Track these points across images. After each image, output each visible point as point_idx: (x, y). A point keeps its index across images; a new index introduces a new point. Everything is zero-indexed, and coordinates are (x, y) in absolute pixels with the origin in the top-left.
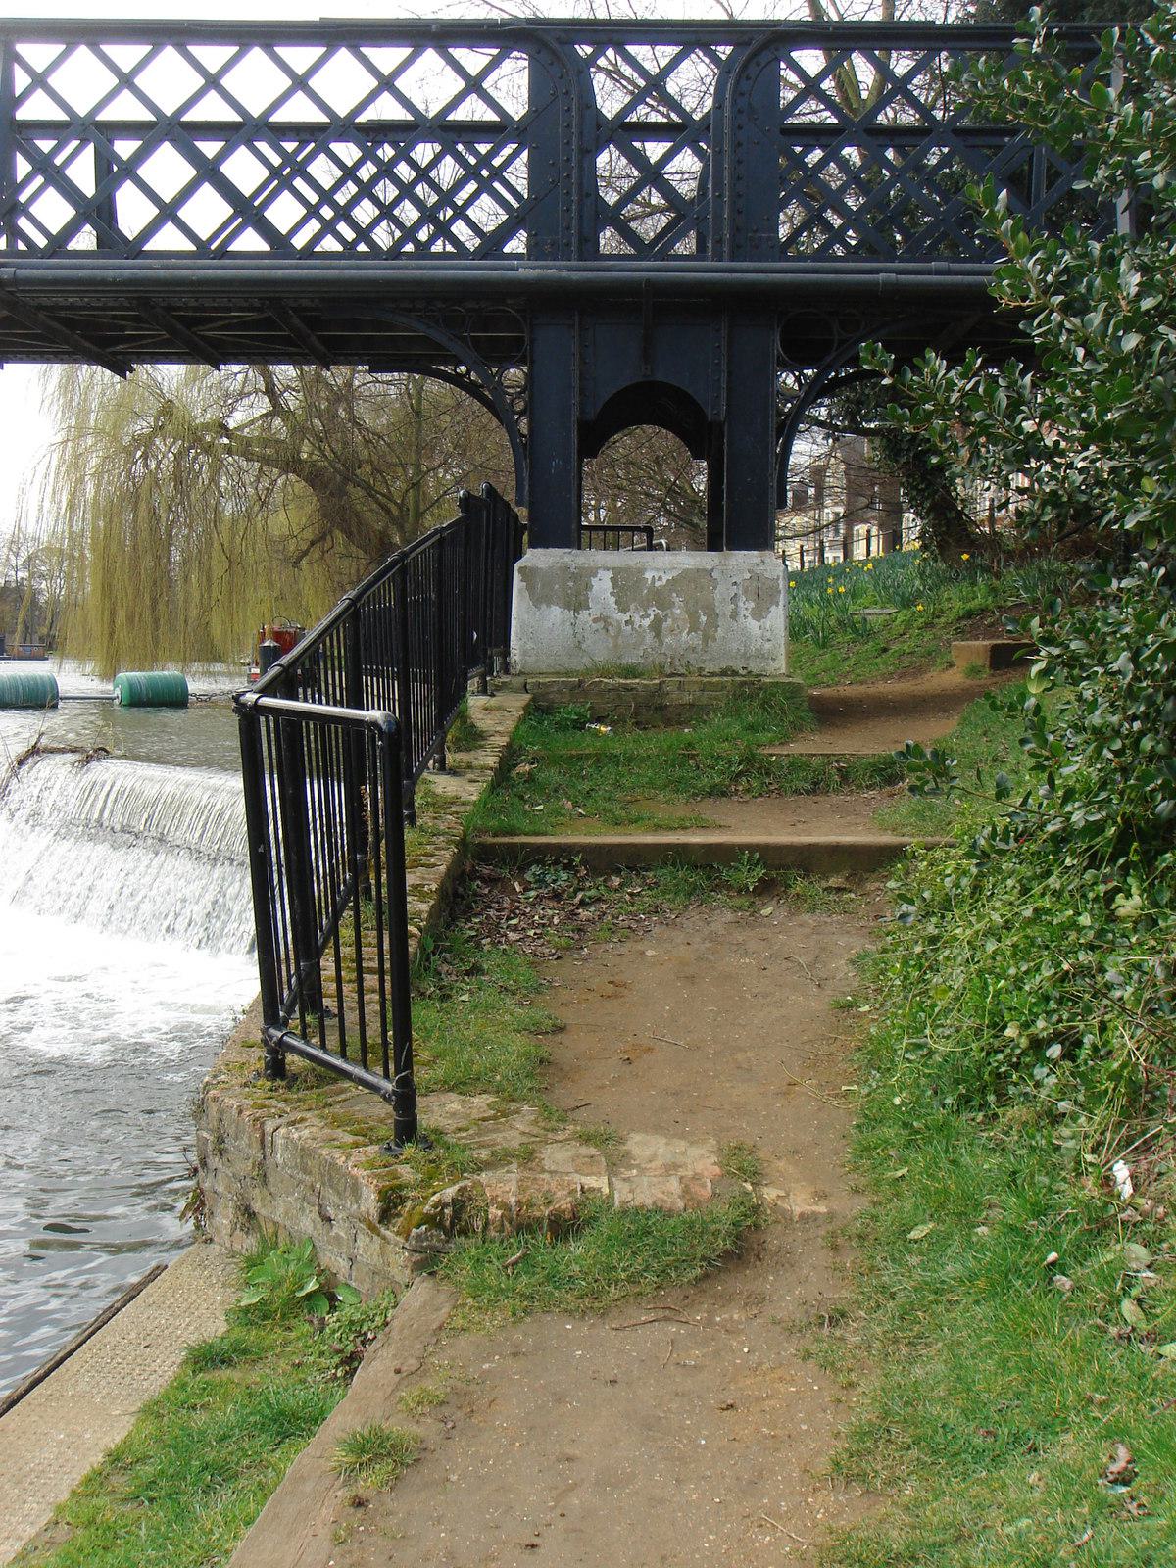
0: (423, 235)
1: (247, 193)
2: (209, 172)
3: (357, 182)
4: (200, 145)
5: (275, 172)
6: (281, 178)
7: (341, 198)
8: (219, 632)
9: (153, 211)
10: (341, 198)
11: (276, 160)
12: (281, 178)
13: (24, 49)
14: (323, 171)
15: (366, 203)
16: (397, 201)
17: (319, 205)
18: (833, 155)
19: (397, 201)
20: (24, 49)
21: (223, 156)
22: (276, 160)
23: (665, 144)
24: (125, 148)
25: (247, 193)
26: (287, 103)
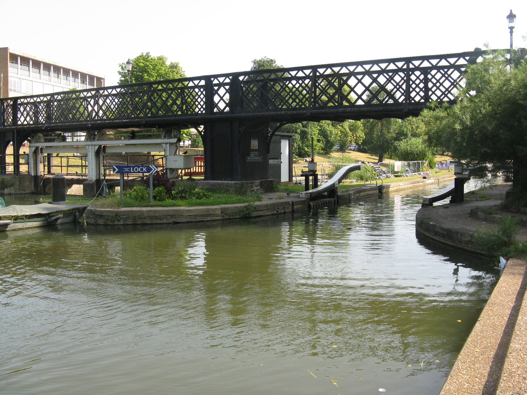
0: (189, 94)
1: (382, 84)
2: (375, 80)
3: (440, 83)
4: (373, 75)
5: (388, 79)
6: (389, 81)
7: (441, 88)
8: (335, 156)
9: (443, 84)
10: (441, 88)
11: (388, 77)
12: (389, 81)
13: (319, 70)
14: (397, 78)
15: (419, 90)
16: (419, 92)
17: (436, 86)
18: (290, 82)
19: (419, 92)
20: (319, 70)
21: (378, 77)
22: (388, 77)
23: (342, 72)
24: (375, 76)
25: (382, 84)
26: (453, 53)
